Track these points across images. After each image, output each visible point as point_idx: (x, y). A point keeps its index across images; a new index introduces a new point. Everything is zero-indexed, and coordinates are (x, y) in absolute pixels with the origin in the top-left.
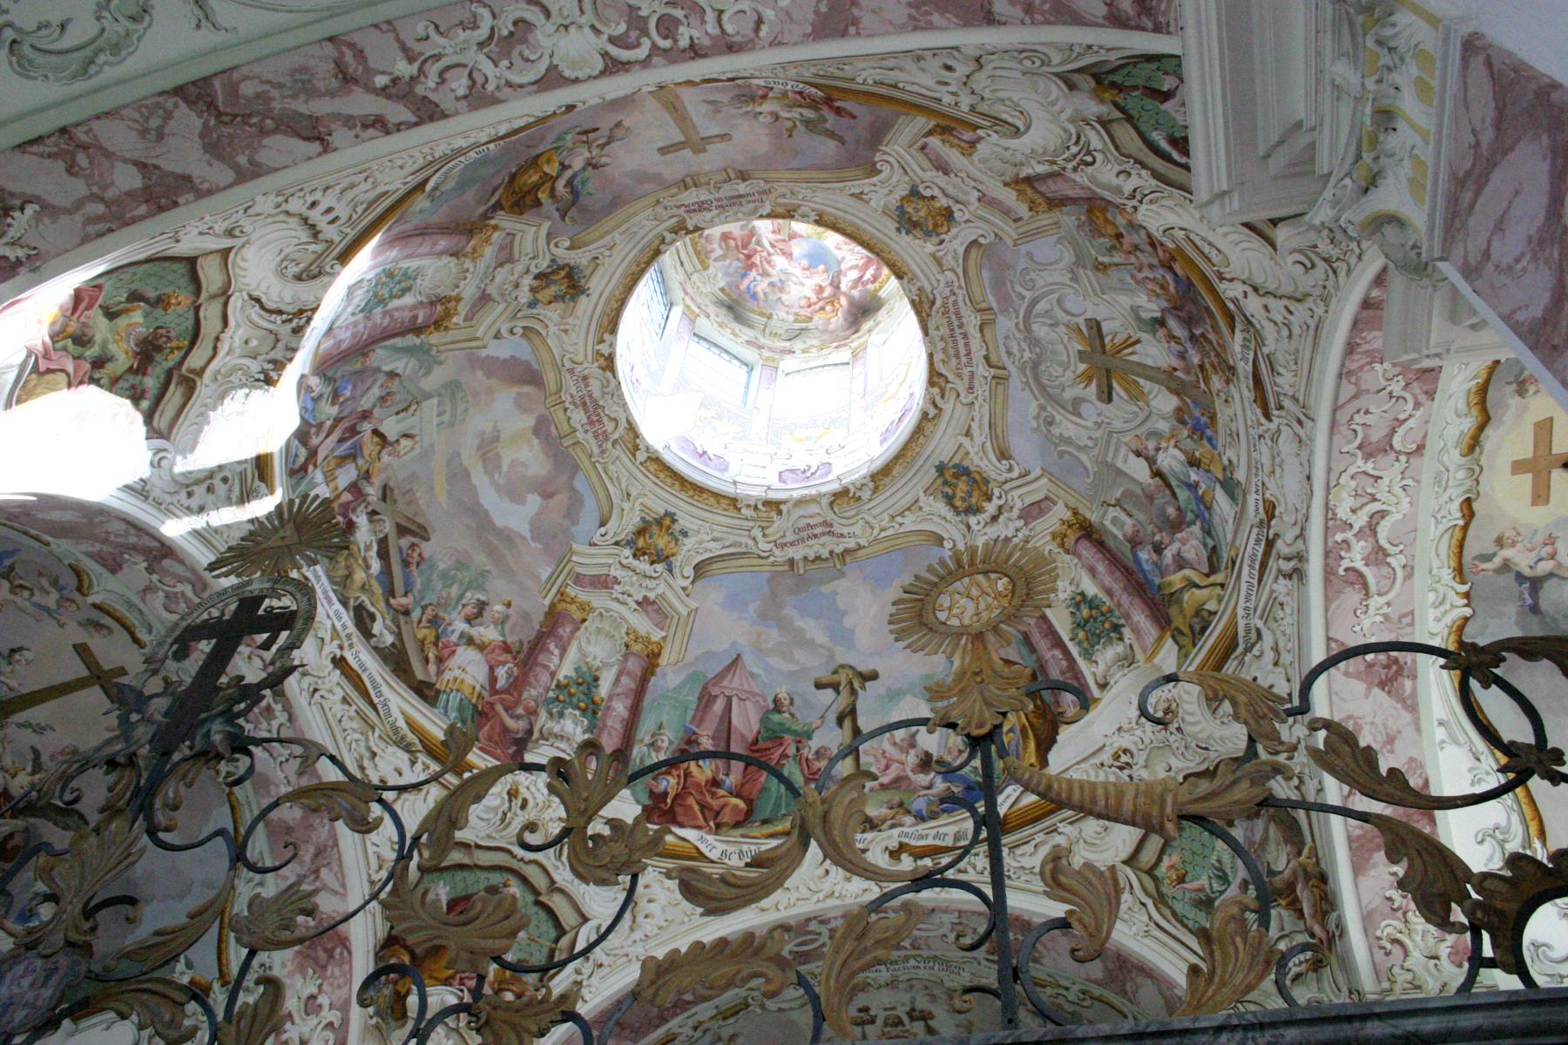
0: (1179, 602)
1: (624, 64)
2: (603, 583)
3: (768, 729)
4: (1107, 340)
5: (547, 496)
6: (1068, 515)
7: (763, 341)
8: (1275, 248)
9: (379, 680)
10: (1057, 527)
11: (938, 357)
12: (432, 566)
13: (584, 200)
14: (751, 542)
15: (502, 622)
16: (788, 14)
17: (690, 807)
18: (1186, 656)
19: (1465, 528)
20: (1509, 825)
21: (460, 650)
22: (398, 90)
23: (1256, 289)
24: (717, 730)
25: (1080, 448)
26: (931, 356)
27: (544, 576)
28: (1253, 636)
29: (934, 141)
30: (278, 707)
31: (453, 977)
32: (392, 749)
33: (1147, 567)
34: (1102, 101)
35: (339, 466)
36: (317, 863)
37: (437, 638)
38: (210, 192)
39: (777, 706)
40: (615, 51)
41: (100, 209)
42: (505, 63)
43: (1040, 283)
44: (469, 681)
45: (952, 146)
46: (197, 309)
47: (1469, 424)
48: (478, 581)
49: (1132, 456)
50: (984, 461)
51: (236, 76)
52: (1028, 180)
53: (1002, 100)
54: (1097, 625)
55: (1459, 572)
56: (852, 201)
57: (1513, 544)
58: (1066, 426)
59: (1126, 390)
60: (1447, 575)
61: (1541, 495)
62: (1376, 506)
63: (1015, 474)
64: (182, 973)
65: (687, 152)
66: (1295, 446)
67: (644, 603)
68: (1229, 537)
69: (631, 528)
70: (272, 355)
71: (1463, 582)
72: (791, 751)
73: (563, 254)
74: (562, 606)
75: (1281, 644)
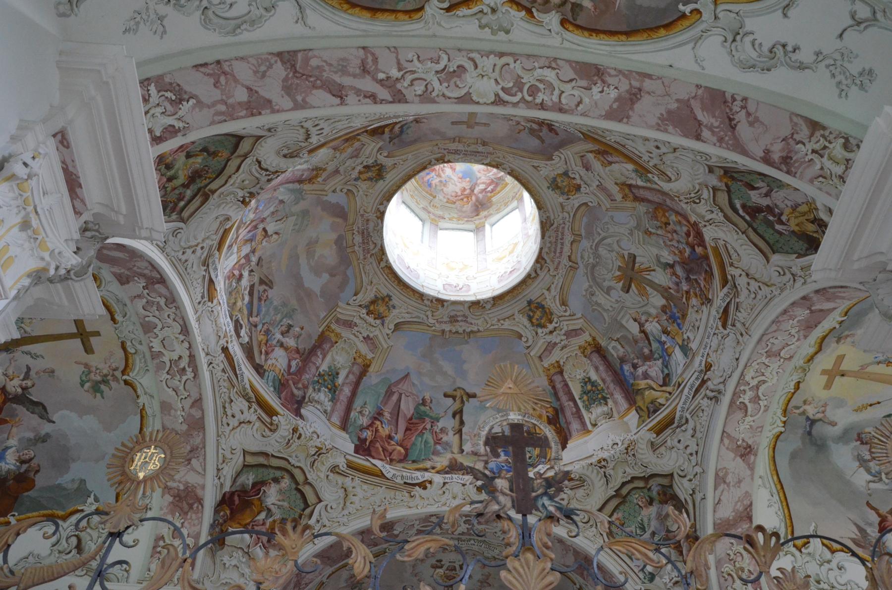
0: (642, 394)
1: (504, 102)
2: (349, 325)
3: (418, 413)
4: (637, 265)
5: (332, 275)
6: (590, 339)
7: (430, 209)
8: (768, 262)
9: (241, 361)
10: (583, 343)
11: (545, 250)
12: (271, 303)
13: (404, 136)
14: (425, 318)
15: (298, 337)
16: (596, 103)
17: (377, 448)
18: (643, 422)
19: (793, 394)
20: (780, 528)
21: (277, 349)
22: (388, 83)
23: (747, 275)
24: (393, 410)
25: (604, 309)
26: (541, 249)
27: (322, 316)
28: (684, 421)
29: (591, 156)
30: (189, 370)
32: (241, 399)
33: (627, 374)
34: (721, 181)
35: (244, 244)
36: (191, 455)
37: (267, 341)
38: (278, 111)
39: (424, 402)
40: (502, 94)
41: (223, 108)
42: (446, 84)
43: (612, 230)
44: (279, 366)
45: (599, 160)
46: (228, 160)
47: (812, 350)
48: (289, 315)
49: (632, 321)
50: (552, 302)
51: (310, 54)
52: (630, 186)
53: (673, 167)
54: (594, 394)
55: (785, 412)
56: (531, 169)
57: (810, 404)
58: (600, 298)
59: (639, 291)
60: (779, 412)
61: (828, 386)
62: (763, 378)
63: (567, 314)
64: (91, 504)
65: (465, 126)
66: (735, 344)
67: (367, 339)
68: (679, 372)
69: (369, 299)
70: (252, 190)
71: (785, 417)
72: (428, 426)
73: (382, 159)
74: (327, 333)
75: (698, 428)
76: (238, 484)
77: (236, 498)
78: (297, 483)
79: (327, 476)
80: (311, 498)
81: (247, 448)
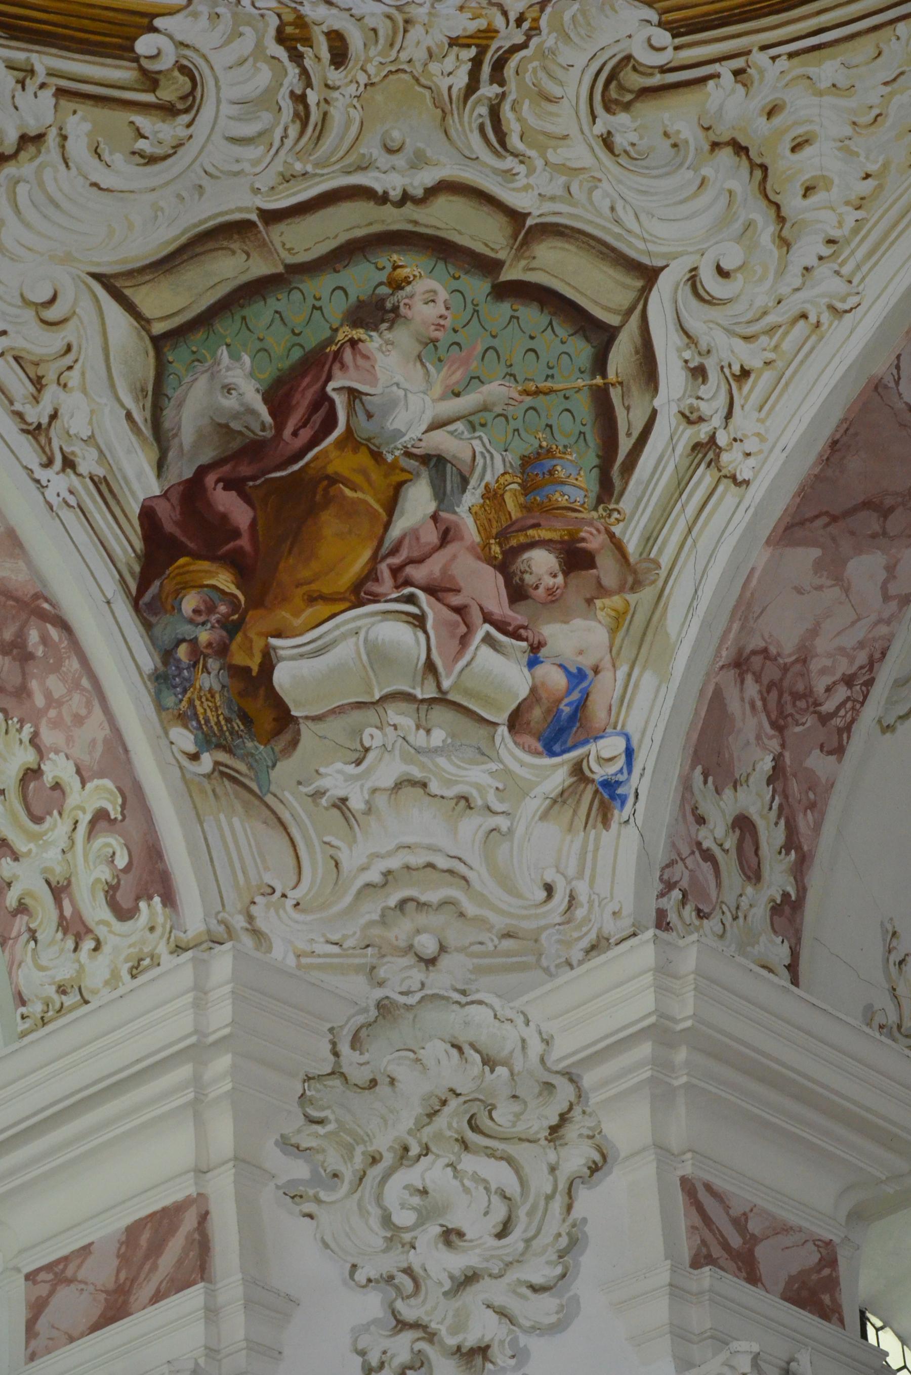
31: (371, 574)
76: (187, 436)
77: (227, 502)
78: (486, 266)
79: (607, 141)
80: (599, 290)
81: (108, 263)
